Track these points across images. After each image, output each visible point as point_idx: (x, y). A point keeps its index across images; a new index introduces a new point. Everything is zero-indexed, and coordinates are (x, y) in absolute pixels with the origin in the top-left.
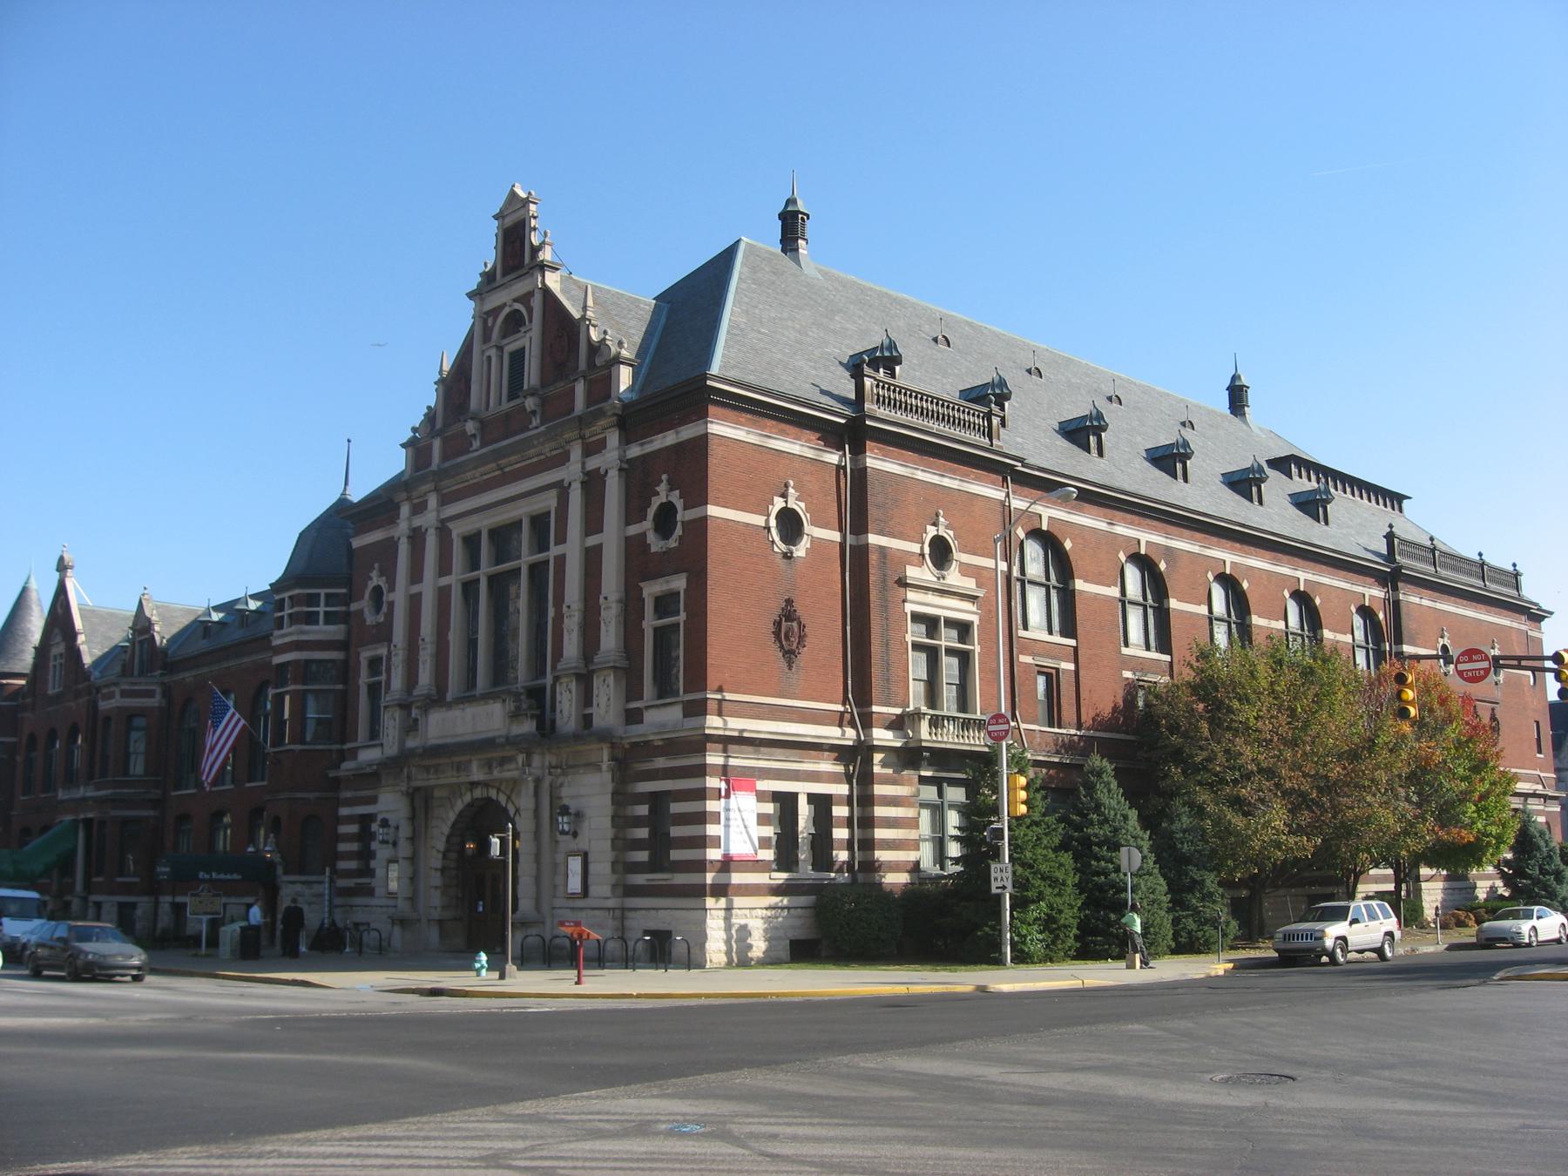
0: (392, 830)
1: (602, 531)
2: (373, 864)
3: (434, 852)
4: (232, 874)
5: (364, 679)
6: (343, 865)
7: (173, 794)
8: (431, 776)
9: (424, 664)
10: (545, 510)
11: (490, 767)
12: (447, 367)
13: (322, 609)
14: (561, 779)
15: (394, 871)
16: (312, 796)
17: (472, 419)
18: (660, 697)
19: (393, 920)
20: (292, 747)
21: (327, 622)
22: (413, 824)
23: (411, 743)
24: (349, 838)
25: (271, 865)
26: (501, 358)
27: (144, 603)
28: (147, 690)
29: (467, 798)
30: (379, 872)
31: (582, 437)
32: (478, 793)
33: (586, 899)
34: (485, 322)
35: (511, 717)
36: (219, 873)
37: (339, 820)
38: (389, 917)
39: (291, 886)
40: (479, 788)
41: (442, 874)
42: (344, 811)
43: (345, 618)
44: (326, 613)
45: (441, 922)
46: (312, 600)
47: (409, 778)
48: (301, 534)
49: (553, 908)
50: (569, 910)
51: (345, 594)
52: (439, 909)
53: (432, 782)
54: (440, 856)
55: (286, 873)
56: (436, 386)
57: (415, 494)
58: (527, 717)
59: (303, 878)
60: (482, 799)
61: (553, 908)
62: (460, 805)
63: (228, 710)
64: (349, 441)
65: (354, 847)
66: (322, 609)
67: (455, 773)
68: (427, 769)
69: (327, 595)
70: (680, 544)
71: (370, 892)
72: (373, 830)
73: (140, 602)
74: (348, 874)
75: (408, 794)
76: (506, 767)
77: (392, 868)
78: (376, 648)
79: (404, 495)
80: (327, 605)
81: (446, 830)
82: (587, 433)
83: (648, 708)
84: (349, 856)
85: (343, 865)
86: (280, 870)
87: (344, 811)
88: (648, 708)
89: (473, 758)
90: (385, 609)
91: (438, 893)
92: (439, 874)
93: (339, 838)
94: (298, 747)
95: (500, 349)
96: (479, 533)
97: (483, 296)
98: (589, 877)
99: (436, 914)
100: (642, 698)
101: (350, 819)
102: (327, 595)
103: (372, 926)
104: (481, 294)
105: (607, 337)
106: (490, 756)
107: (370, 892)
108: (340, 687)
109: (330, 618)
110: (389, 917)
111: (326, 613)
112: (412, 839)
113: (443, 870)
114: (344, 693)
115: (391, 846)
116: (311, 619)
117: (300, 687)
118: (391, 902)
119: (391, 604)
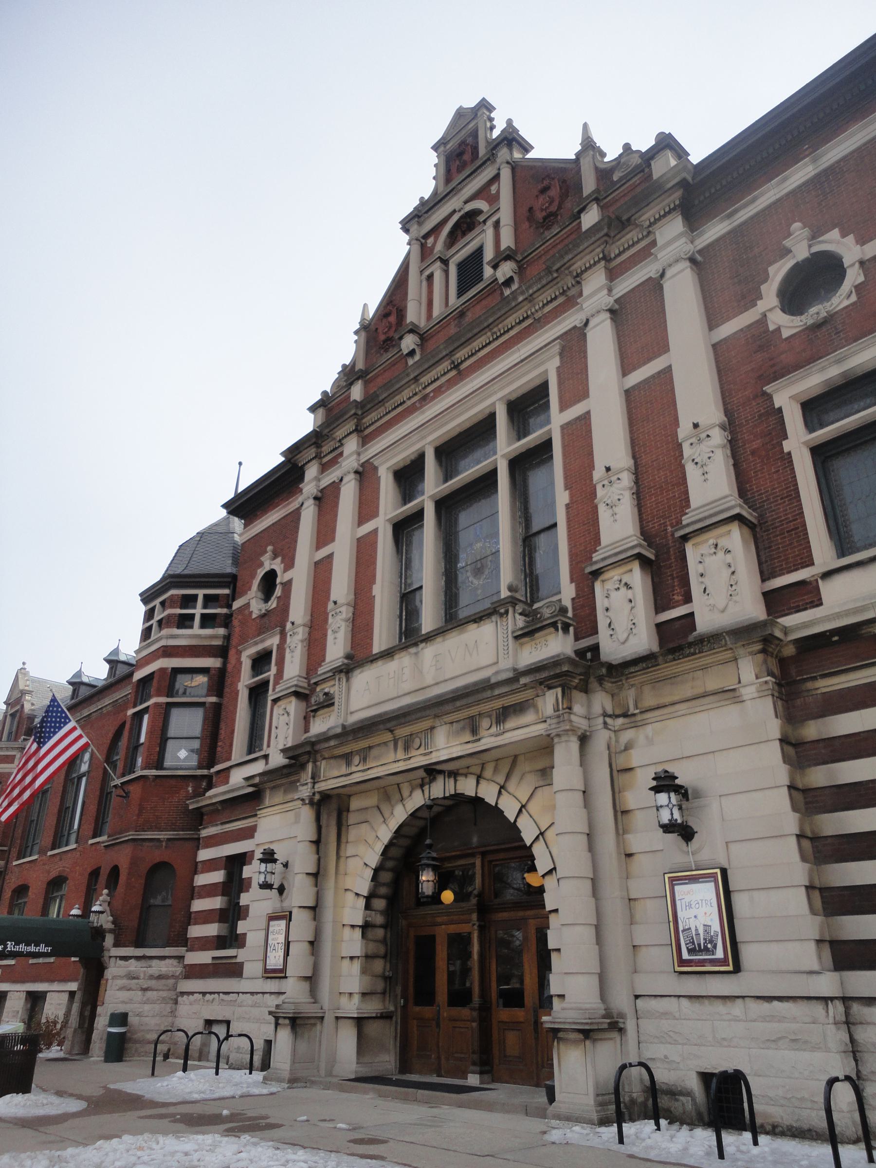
0: (278, 867)
1: (668, 350)
2: (242, 927)
3: (350, 896)
4: (28, 944)
5: (245, 679)
6: (196, 931)
7: (15, 863)
8: (354, 769)
9: (334, 632)
10: (538, 382)
11: (474, 731)
12: (371, 312)
13: (198, 611)
14: (627, 736)
15: (278, 933)
16: (163, 835)
17: (411, 331)
18: (841, 554)
19: (277, 1019)
20: (146, 772)
21: (203, 626)
22: (318, 852)
23: (320, 726)
24: (209, 891)
25: (99, 933)
26: (446, 272)
27: (20, 676)
28: (7, 756)
29: (417, 800)
30: (254, 939)
31: (606, 258)
32: (439, 789)
33: (739, 974)
34: (423, 246)
35: (517, 638)
36: (17, 944)
37: (196, 868)
38: (270, 1013)
39: (122, 963)
40: (440, 780)
41: (363, 936)
42: (204, 855)
43: (226, 621)
44: (203, 616)
45: (360, 1022)
46: (189, 601)
47: (315, 777)
48: (180, 546)
49: (637, 997)
50: (684, 1001)
51: (228, 595)
52: (356, 999)
53: (357, 777)
54: (362, 902)
55: (117, 944)
56: (356, 338)
57: (326, 449)
58: (557, 630)
59: (140, 952)
60: (445, 798)
61: (637, 997)
62: (399, 815)
63: (65, 723)
64: (240, 464)
65: (216, 903)
66: (198, 611)
67: (401, 754)
68: (347, 758)
69: (206, 597)
70: (865, 276)
71: (234, 970)
72: (245, 875)
73: (17, 676)
74: (204, 944)
75: (311, 803)
76: (510, 724)
77: (276, 928)
78: (263, 641)
79: (312, 452)
80: (205, 606)
81: (374, 859)
82: (614, 250)
83: (828, 575)
84: (206, 917)
85: (196, 931)
86: (109, 940)
87: (204, 855)
88: (828, 575)
89: (437, 722)
90: (278, 591)
91: (356, 966)
92: (358, 933)
93: (193, 893)
94: (154, 772)
95: (445, 262)
96: (420, 459)
97: (422, 219)
98: (735, 921)
99: (352, 1007)
100: (812, 564)
101: (211, 865)
102: (206, 597)
103: (235, 1029)
104: (419, 217)
105: (557, 293)
106: (474, 711)
107: (234, 970)
108: (213, 699)
109: (207, 621)
110: (270, 1013)
111: (203, 616)
112: (316, 876)
113: (366, 927)
114: (222, 673)
115: (275, 892)
116: (185, 621)
117: (163, 700)
118: (272, 986)
119: (288, 585)
